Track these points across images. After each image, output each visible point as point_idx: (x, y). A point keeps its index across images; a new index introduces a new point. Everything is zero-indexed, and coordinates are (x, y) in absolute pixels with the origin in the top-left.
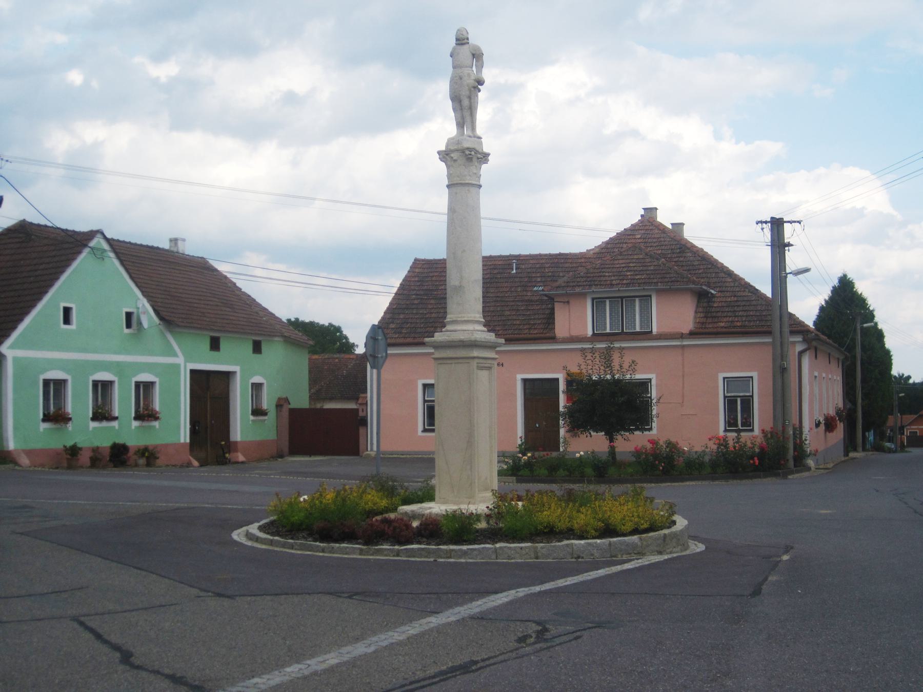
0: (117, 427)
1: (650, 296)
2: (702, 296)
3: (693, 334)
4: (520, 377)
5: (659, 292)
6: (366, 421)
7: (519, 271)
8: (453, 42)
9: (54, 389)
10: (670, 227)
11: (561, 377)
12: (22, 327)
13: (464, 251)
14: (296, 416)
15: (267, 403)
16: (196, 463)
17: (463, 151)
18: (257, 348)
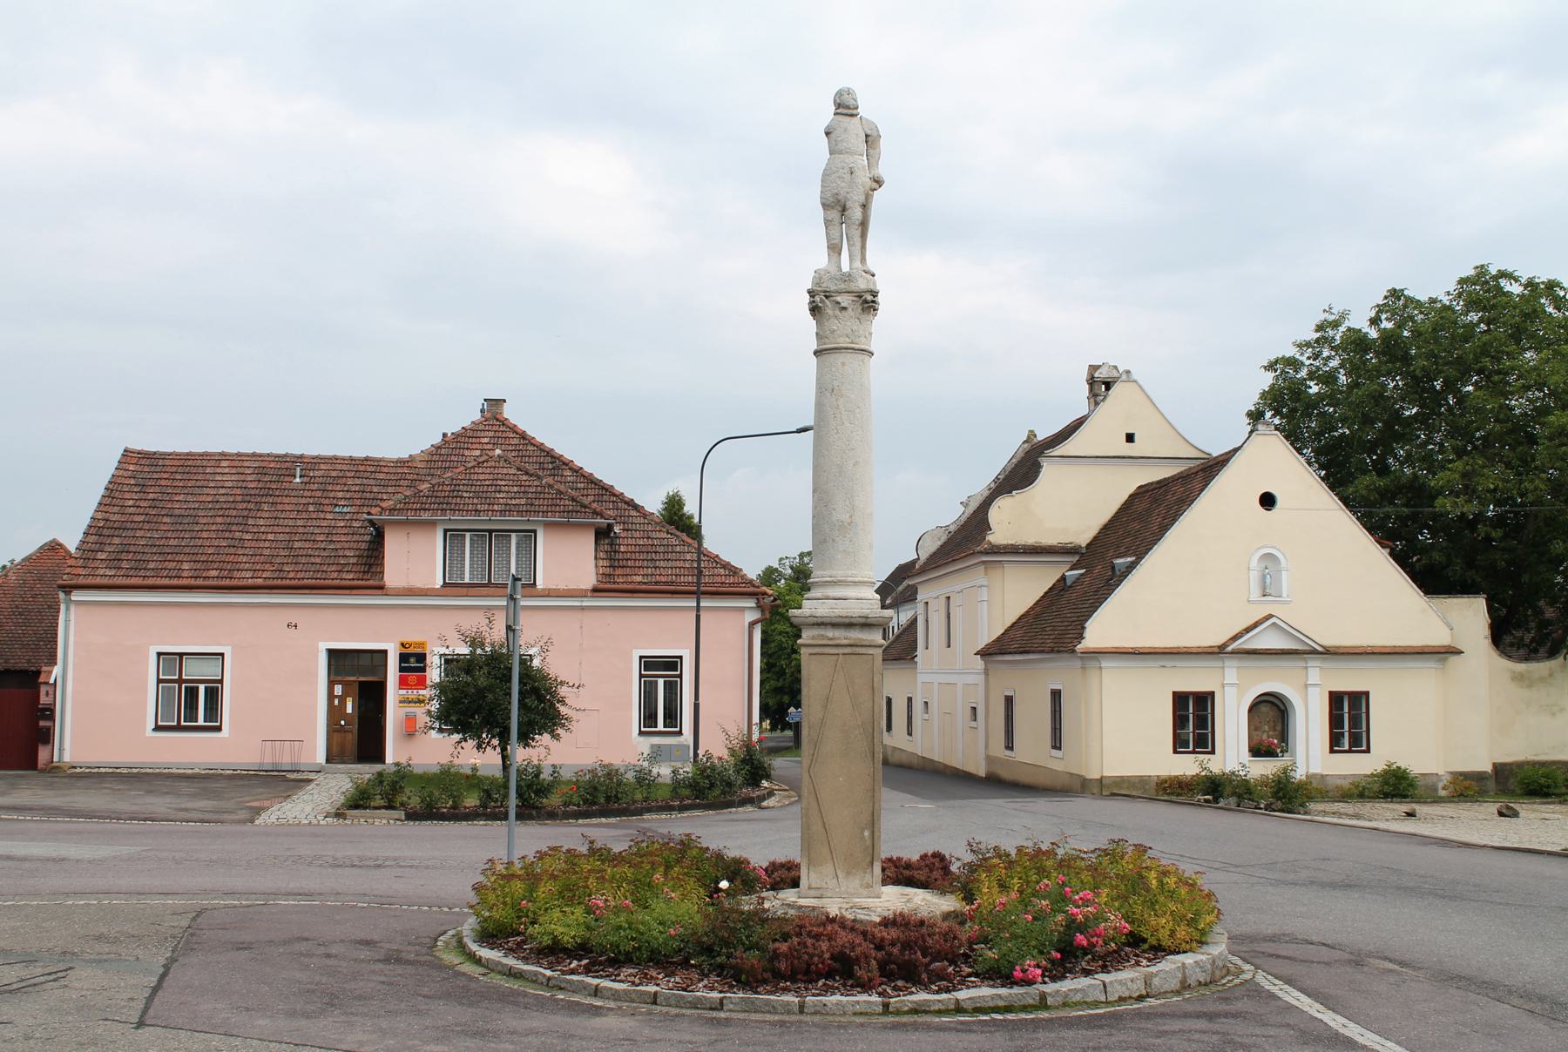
1: (535, 532)
2: (603, 534)
3: (596, 591)
4: (325, 645)
5: (547, 525)
6: (53, 711)
8: (827, 113)
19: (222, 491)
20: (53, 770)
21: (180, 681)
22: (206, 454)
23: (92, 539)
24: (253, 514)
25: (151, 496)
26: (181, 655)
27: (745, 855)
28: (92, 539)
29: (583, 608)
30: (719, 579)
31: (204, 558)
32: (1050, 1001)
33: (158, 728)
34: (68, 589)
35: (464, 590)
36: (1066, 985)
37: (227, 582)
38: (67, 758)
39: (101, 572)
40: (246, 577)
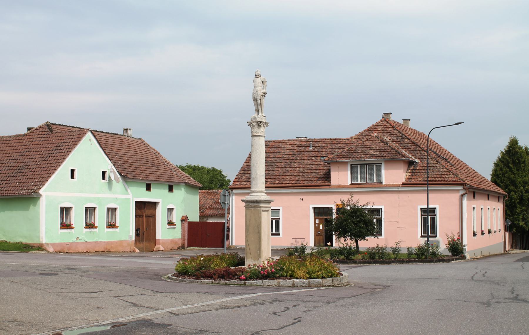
4: (312, 206)
7: (314, 148)
10: (402, 122)
11: (334, 207)
14: (192, 226)
15: (176, 218)
16: (137, 251)
17: (257, 122)
18: (171, 189)
19: (286, 153)
23: (242, 172)
24: (294, 161)
28: (242, 172)
29: (399, 191)
30: (450, 179)
31: (275, 177)
35: (357, 186)
37: (281, 185)
39: (243, 183)
40: (287, 183)
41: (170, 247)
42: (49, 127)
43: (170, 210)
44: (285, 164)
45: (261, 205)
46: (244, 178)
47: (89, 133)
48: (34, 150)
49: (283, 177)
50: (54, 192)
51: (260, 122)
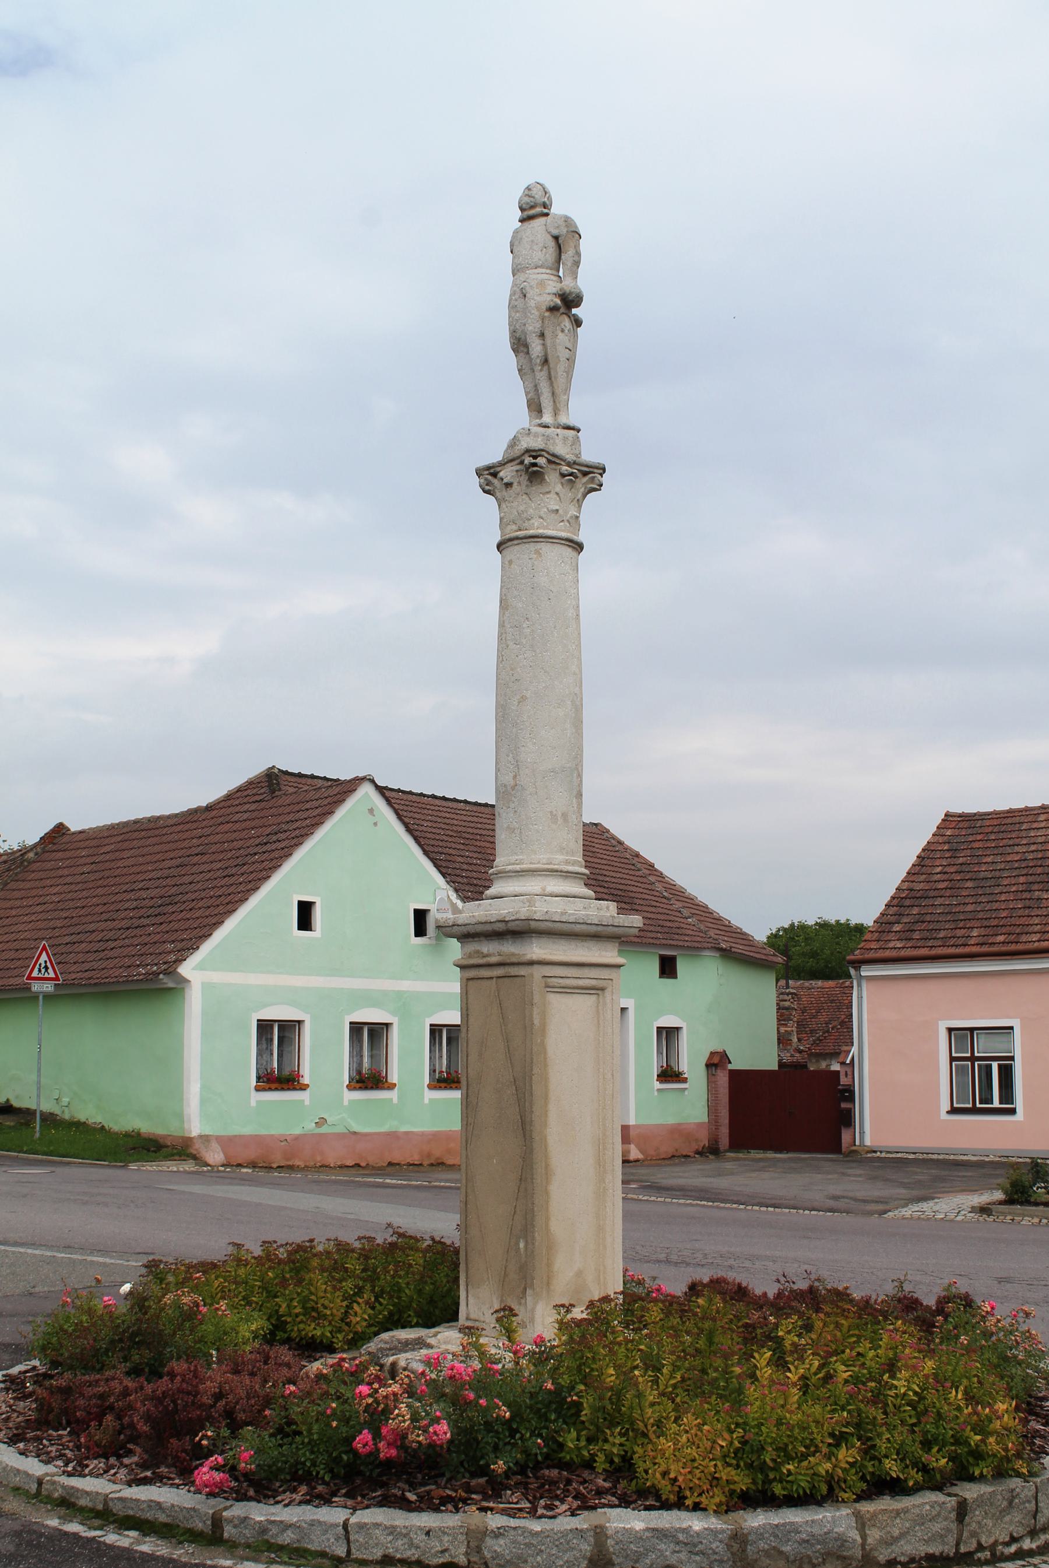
0: (395, 1101)
6: (852, 1093)
9: (278, 1036)
12: (219, 935)
13: (523, 699)
18: (668, 968)
19: (1033, 848)
20: (857, 1157)
21: (973, 1059)
22: (1027, 809)
25: (961, 860)
26: (972, 1030)
27: (720, 1273)
31: (994, 922)
32: (228, 1531)
33: (954, 1111)
34: (858, 964)
36: (259, 1513)
37: (1013, 947)
38: (868, 1142)
39: (891, 945)
40: (1033, 941)
41: (667, 1149)
42: (273, 780)
43: (668, 1035)
44: (1031, 879)
45: (537, 950)
46: (897, 928)
47: (366, 789)
48: (214, 848)
49: (1022, 921)
50: (237, 970)
51: (535, 453)
